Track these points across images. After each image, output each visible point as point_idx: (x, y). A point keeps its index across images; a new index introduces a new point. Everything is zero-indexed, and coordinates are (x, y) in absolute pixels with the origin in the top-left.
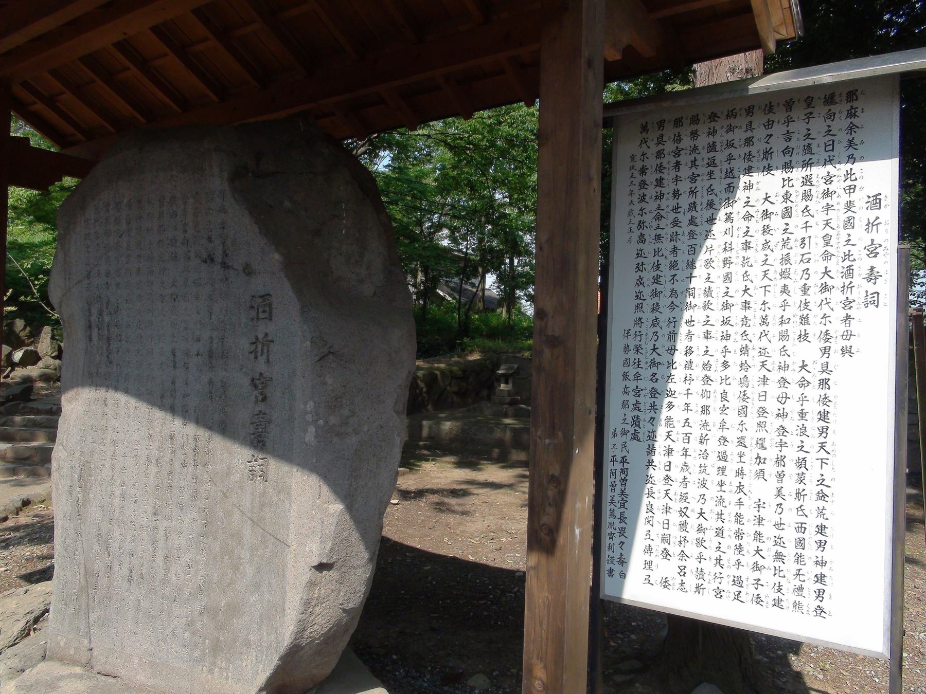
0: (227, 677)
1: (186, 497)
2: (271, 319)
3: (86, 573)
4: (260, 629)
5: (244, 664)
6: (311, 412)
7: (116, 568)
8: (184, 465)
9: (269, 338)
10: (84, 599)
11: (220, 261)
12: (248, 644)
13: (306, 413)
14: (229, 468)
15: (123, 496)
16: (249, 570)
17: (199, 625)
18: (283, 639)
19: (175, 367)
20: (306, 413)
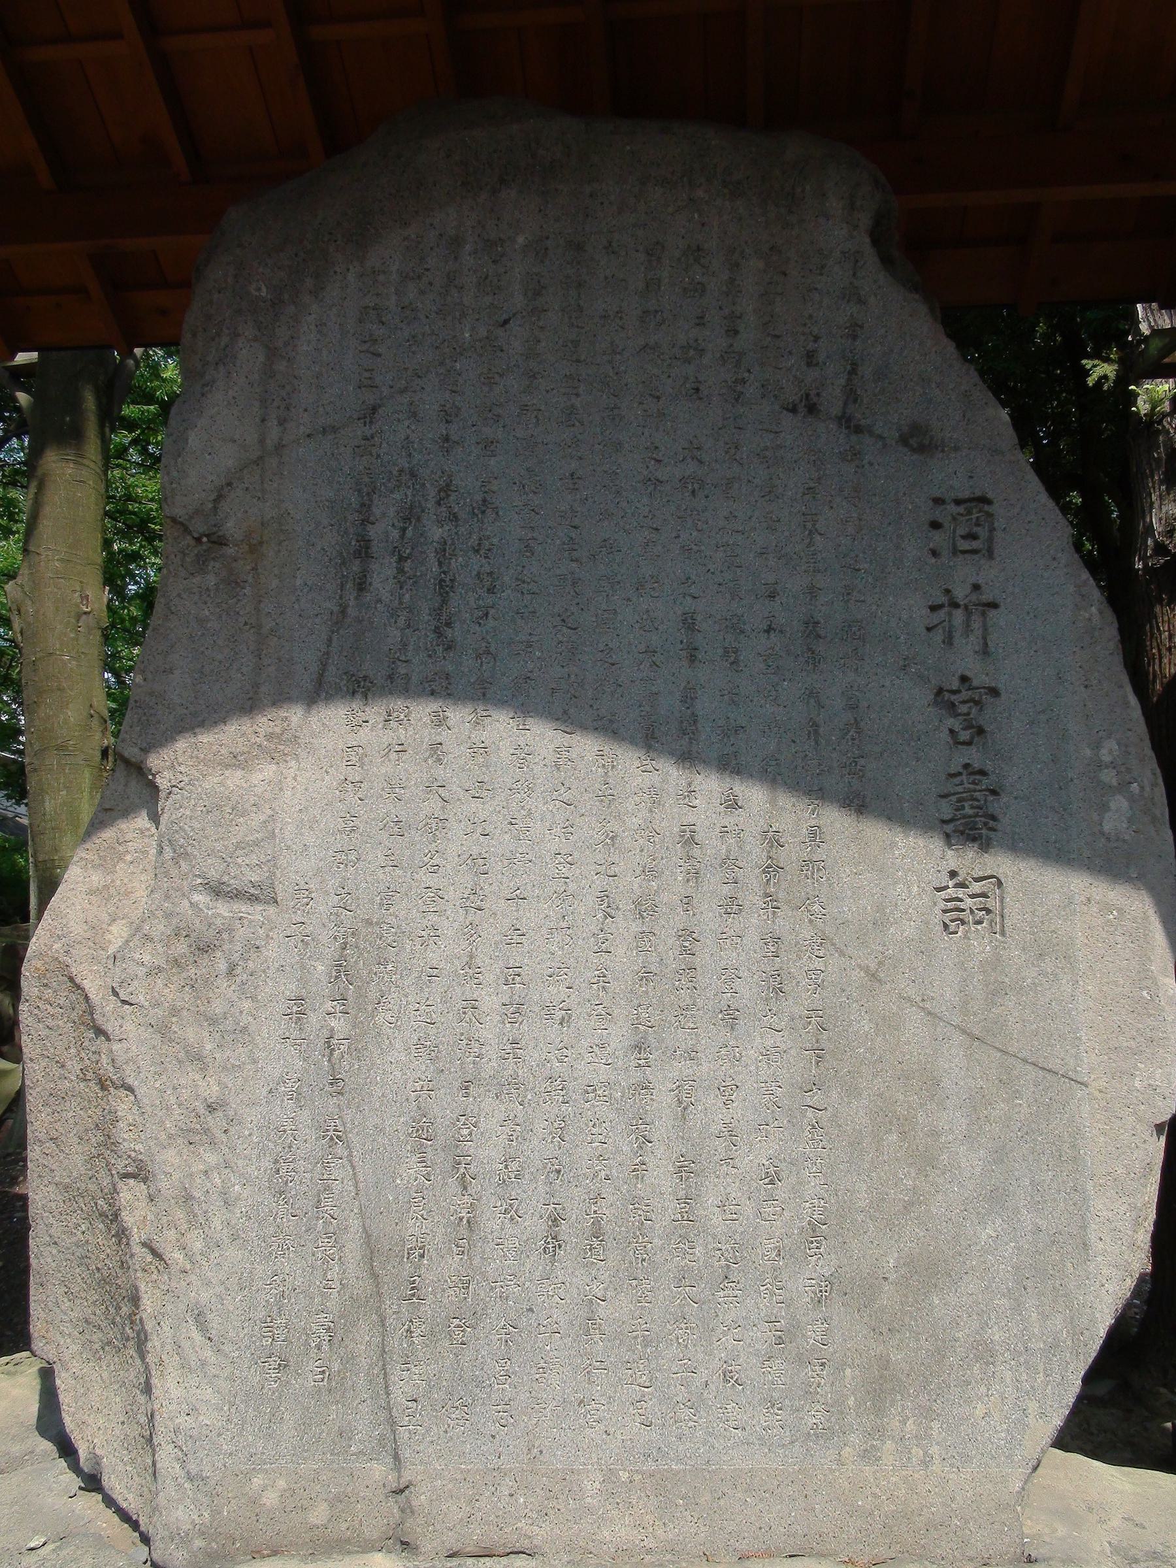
0: (926, 1462)
1: (748, 991)
2: (990, 554)
3: (371, 1249)
4: (1018, 1307)
5: (980, 1410)
6: (1113, 765)
7: (492, 1222)
8: (732, 906)
9: (986, 597)
10: (364, 1338)
11: (836, 411)
12: (985, 1353)
13: (1100, 766)
14: (880, 908)
15: (515, 1011)
16: (971, 1162)
17: (813, 1334)
18: (1093, 1320)
19: (692, 659)
20: (1100, 766)
